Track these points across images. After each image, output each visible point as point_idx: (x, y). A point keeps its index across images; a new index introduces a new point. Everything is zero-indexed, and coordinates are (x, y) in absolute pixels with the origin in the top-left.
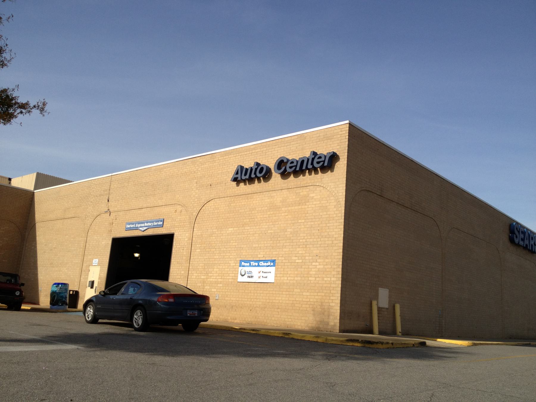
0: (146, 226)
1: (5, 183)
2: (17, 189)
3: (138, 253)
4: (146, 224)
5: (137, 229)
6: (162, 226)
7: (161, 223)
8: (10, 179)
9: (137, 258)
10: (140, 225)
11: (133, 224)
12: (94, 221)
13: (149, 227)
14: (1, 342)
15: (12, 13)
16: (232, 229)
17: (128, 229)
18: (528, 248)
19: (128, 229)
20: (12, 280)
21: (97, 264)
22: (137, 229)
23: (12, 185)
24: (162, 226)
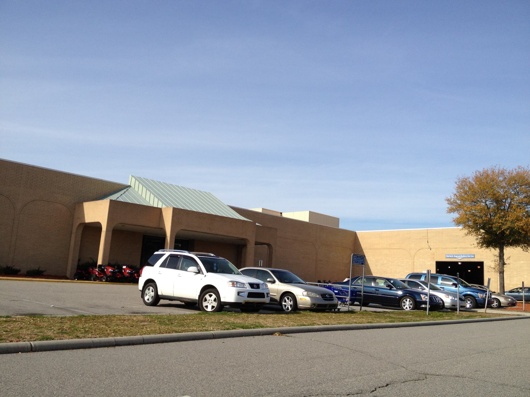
0: (462, 257)
1: (280, 215)
2: (114, 183)
3: (470, 270)
4: (461, 256)
5: (455, 258)
6: (474, 257)
7: (473, 256)
8: (281, 213)
9: (469, 272)
10: (457, 256)
11: (451, 255)
12: (418, 252)
13: (464, 258)
14: (1, 355)
15: (529, 254)
16: (522, 262)
17: (447, 258)
18: (262, 261)
19: (447, 258)
20: (119, 277)
21: (107, 265)
22: (455, 258)
23: (283, 216)
24: (474, 257)
